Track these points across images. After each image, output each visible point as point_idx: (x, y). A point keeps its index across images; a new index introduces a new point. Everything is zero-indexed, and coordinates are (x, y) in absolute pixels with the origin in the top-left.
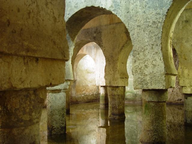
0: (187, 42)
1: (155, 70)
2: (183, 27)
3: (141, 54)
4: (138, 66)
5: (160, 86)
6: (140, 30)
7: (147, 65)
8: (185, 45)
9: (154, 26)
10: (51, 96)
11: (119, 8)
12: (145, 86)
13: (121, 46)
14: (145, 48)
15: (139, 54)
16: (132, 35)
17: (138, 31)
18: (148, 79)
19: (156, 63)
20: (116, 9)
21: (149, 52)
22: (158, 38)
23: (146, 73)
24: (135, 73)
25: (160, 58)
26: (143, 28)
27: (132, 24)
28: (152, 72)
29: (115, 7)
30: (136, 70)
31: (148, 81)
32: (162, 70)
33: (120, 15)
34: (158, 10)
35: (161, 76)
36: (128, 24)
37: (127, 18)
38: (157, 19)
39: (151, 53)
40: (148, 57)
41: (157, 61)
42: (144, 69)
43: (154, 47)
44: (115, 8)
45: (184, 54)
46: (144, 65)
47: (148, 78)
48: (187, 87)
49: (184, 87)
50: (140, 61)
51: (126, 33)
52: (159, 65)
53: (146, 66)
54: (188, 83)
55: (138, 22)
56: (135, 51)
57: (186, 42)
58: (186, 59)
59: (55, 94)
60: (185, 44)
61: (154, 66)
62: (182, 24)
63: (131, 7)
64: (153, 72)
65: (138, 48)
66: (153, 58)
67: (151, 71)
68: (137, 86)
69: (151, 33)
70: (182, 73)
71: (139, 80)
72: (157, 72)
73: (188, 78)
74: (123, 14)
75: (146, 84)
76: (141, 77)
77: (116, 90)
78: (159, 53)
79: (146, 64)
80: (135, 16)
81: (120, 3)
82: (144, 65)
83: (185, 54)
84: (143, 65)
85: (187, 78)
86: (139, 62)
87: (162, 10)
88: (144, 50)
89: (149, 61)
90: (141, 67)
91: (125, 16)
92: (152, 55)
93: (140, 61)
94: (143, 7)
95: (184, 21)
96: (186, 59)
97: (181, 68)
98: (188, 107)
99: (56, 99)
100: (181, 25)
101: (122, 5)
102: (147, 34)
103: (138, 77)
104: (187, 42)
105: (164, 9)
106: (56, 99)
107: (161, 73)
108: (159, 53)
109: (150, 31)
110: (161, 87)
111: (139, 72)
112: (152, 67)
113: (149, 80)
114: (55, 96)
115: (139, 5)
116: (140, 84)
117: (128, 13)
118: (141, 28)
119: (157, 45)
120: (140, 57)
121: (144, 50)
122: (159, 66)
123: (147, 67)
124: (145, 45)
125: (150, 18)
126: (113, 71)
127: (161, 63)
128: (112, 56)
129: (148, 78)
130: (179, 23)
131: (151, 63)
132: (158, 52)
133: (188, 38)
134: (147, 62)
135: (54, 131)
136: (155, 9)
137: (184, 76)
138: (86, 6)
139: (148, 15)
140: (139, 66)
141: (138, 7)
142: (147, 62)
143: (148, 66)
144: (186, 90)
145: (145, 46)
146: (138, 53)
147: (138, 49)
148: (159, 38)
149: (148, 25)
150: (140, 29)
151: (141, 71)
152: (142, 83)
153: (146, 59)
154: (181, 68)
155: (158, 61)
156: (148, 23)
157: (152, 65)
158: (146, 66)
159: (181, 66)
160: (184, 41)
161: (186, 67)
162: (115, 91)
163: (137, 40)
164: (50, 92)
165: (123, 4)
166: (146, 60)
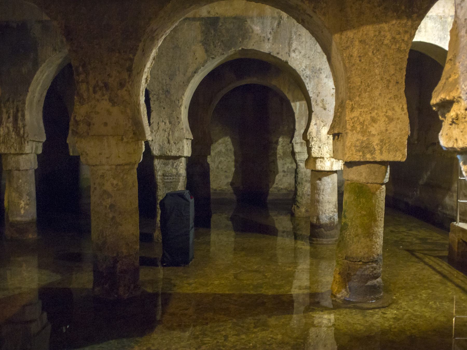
4: (358, 118)
5: (398, 156)
7: (376, 116)
8: (325, 83)
13: (191, 70)
19: (393, 114)
23: (373, 132)
25: (401, 106)
28: (384, 131)
40: (379, 102)
41: (396, 112)
42: (369, 124)
45: (322, 98)
48: (325, 159)
49: (319, 159)
51: (203, 45)
52: (398, 119)
54: (327, 152)
57: (326, 77)
58: (325, 109)
64: (387, 130)
65: (359, 84)
71: (358, 144)
73: (328, 143)
76: (362, 138)
77: (175, 165)
79: (374, 114)
82: (371, 117)
83: (325, 100)
85: (326, 142)
90: (364, 121)
92: (386, 100)
93: (361, 109)
96: (325, 109)
97: (316, 124)
102: (378, 59)
103: (355, 139)
109: (386, 55)
111: (358, 129)
113: (377, 145)
122: (399, 121)
126: (170, 123)
127: (403, 115)
128: (167, 91)
131: (383, 114)
132: (399, 96)
134: (376, 111)
140: (360, 118)
143: (378, 118)
144: (322, 164)
147: (360, 86)
148: (401, 69)
151: (363, 128)
153: (376, 106)
154: (316, 124)
157: (385, 117)
159: (316, 121)
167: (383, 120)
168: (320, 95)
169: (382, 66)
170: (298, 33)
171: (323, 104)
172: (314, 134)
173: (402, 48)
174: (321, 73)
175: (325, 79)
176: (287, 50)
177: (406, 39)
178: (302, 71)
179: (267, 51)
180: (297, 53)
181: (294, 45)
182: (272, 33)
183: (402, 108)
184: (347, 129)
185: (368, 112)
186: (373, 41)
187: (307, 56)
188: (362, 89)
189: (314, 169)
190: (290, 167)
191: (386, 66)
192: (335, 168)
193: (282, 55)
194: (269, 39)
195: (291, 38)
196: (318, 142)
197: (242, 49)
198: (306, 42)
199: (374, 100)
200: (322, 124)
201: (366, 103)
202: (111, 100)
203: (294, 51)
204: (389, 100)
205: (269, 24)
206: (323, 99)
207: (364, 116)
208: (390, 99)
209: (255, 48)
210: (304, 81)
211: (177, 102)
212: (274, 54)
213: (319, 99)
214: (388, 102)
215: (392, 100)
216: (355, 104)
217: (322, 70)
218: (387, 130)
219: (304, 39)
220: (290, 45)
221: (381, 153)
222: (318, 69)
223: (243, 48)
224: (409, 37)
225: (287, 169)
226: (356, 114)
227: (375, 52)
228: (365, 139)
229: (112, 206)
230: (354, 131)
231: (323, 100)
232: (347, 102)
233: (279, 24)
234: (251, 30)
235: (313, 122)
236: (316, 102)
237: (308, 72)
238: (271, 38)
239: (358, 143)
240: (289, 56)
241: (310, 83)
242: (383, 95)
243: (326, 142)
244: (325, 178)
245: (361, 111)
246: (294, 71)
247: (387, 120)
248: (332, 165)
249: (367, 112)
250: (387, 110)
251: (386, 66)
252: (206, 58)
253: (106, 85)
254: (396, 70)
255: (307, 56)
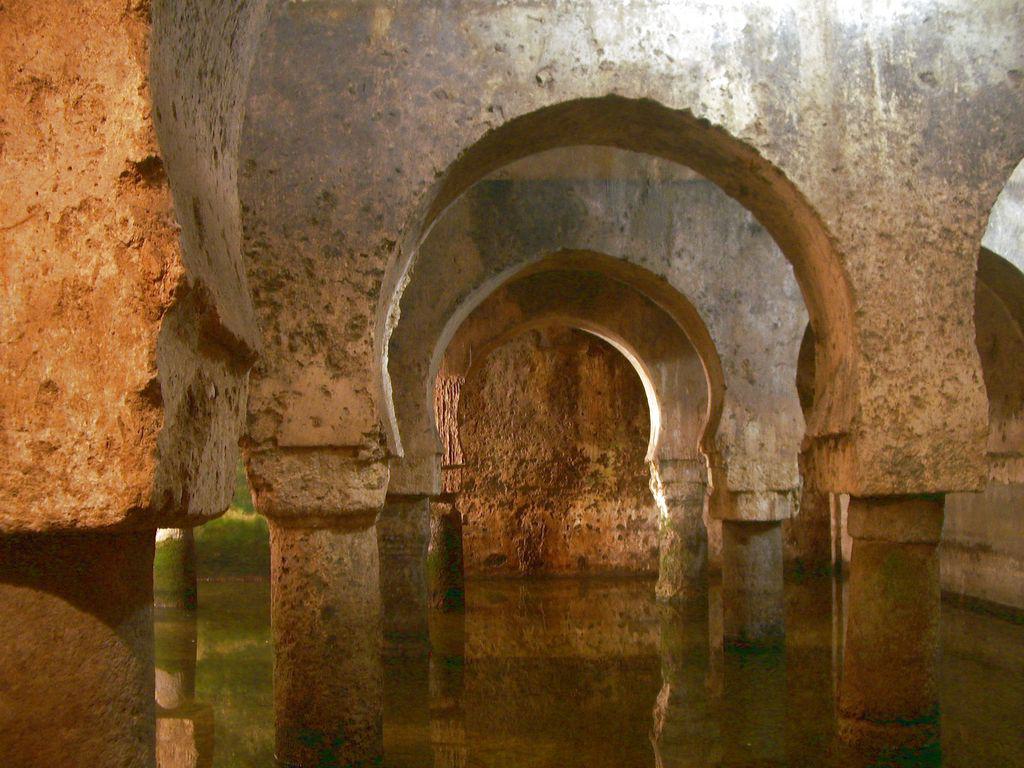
0: (756, 310)
1: (953, 420)
2: (741, 249)
3: (898, 349)
4: (886, 401)
6: (893, 254)
9: (947, 246)
10: (327, 549)
11: (794, 142)
12: (909, 480)
14: (915, 328)
15: (886, 350)
16: (858, 269)
17: (883, 256)
18: (923, 454)
19: (956, 389)
20: (780, 142)
21: (927, 347)
22: (963, 294)
23: (918, 430)
24: (871, 427)
26: (905, 247)
27: (855, 222)
29: (775, 133)
30: (877, 416)
31: (924, 462)
32: (981, 419)
33: (799, 172)
34: (964, 190)
35: (974, 442)
36: (836, 217)
37: (833, 193)
38: (957, 220)
39: (937, 351)
40: (926, 363)
41: (962, 384)
43: (948, 326)
44: (771, 136)
46: (912, 397)
47: (923, 449)
48: (758, 494)
49: (743, 495)
50: (892, 378)
53: (917, 401)
54: (761, 479)
55: (884, 221)
56: (873, 335)
58: (752, 382)
59: (349, 538)
60: (751, 318)
61: (951, 401)
62: (739, 236)
63: (852, 150)
64: (945, 424)
66: (946, 371)
67: (939, 422)
68: (876, 480)
69: (937, 272)
70: (737, 439)
72: (960, 426)
73: (761, 458)
74: (814, 174)
75: (916, 471)
76: (894, 443)
77: (411, 514)
78: (969, 353)
79: (916, 391)
80: (869, 194)
81: (800, 120)
82: (912, 397)
83: (751, 360)
84: (907, 396)
86: (888, 382)
87: (976, 193)
88: (910, 338)
89: (929, 380)
91: (822, 183)
92: (941, 359)
93: (892, 378)
94: (903, 163)
95: (746, 226)
96: (752, 382)
97: (733, 416)
98: (754, 577)
99: (357, 563)
100: (733, 240)
101: (810, 134)
102: (919, 273)
103: (881, 446)
104: (759, 312)
105: (983, 188)
106: (357, 563)
107: (977, 429)
108: (969, 353)
109: (933, 265)
110: (972, 482)
111: (887, 423)
112: (940, 404)
113: (926, 457)
114: (351, 546)
115: (887, 150)
116: (890, 473)
117: (834, 170)
118: (895, 246)
119: (960, 322)
120: (891, 361)
121: (910, 338)
123: (920, 406)
124: (911, 317)
125: (930, 211)
127: (977, 391)
129: (923, 449)
130: (727, 230)
131: (936, 389)
132: (966, 351)
133: (760, 297)
134: (921, 384)
135: (354, 743)
136: (950, 182)
137: (744, 450)
138: (610, 91)
139: (925, 200)
140: (889, 399)
141: (883, 158)
142: (921, 384)
144: (750, 506)
145: (912, 321)
146: (884, 346)
148: (965, 294)
149: (925, 238)
150: (889, 250)
152: (899, 468)
154: (733, 416)
155: (965, 383)
156: (924, 230)
158: (917, 401)
159: (733, 410)
160: (745, 308)
161: (752, 414)
162: (404, 516)
163: (881, 291)
164: (320, 528)
165: (815, 129)
166: (917, 376)
167: (936, 403)
168: (740, 350)
169: (927, 287)
170: (686, 216)
171: (747, 371)
172: (730, 439)
173: (964, 252)
174: (739, 302)
175: (749, 315)
176: (663, 251)
177: (971, 231)
178: (699, 298)
179: (618, 254)
180: (686, 259)
181: (679, 242)
182: (629, 215)
183: (974, 376)
184: (864, 425)
185: (906, 387)
186: (905, 236)
187: (708, 265)
188: (889, 338)
189: (730, 518)
190: (633, 518)
191: (934, 289)
192: (778, 515)
193: (652, 264)
194: (622, 229)
195: (671, 226)
196: (739, 458)
197: (564, 249)
198: (706, 236)
199: (917, 360)
200: (748, 416)
201: (900, 368)
202: (331, 363)
203: (679, 256)
204: (947, 361)
205: (622, 194)
206: (748, 361)
207: (897, 395)
208: (948, 356)
209: (593, 246)
210: (705, 320)
211: (416, 370)
212: (636, 261)
213: (739, 361)
214: (944, 364)
215: (953, 361)
216: (877, 370)
217: (741, 295)
218: (945, 424)
219: (699, 229)
220: (669, 241)
221: (936, 475)
222: (733, 293)
223: (567, 247)
224: (977, 227)
225: (628, 522)
226: (880, 390)
227: (911, 258)
228: (901, 445)
229: (327, 611)
230: (879, 429)
231: (746, 363)
232: (861, 364)
233: (644, 195)
234: (582, 209)
235: (727, 412)
236: (732, 367)
237: (712, 301)
238: (628, 227)
239: (886, 454)
240: (670, 265)
241: (717, 325)
242: (934, 349)
243: (758, 456)
244: (756, 537)
245: (891, 385)
246: (681, 297)
247: (944, 402)
248: (772, 506)
249: (903, 386)
250: (943, 381)
251: (934, 289)
252: (482, 269)
253: (321, 331)
254: (955, 295)
255: (708, 265)
